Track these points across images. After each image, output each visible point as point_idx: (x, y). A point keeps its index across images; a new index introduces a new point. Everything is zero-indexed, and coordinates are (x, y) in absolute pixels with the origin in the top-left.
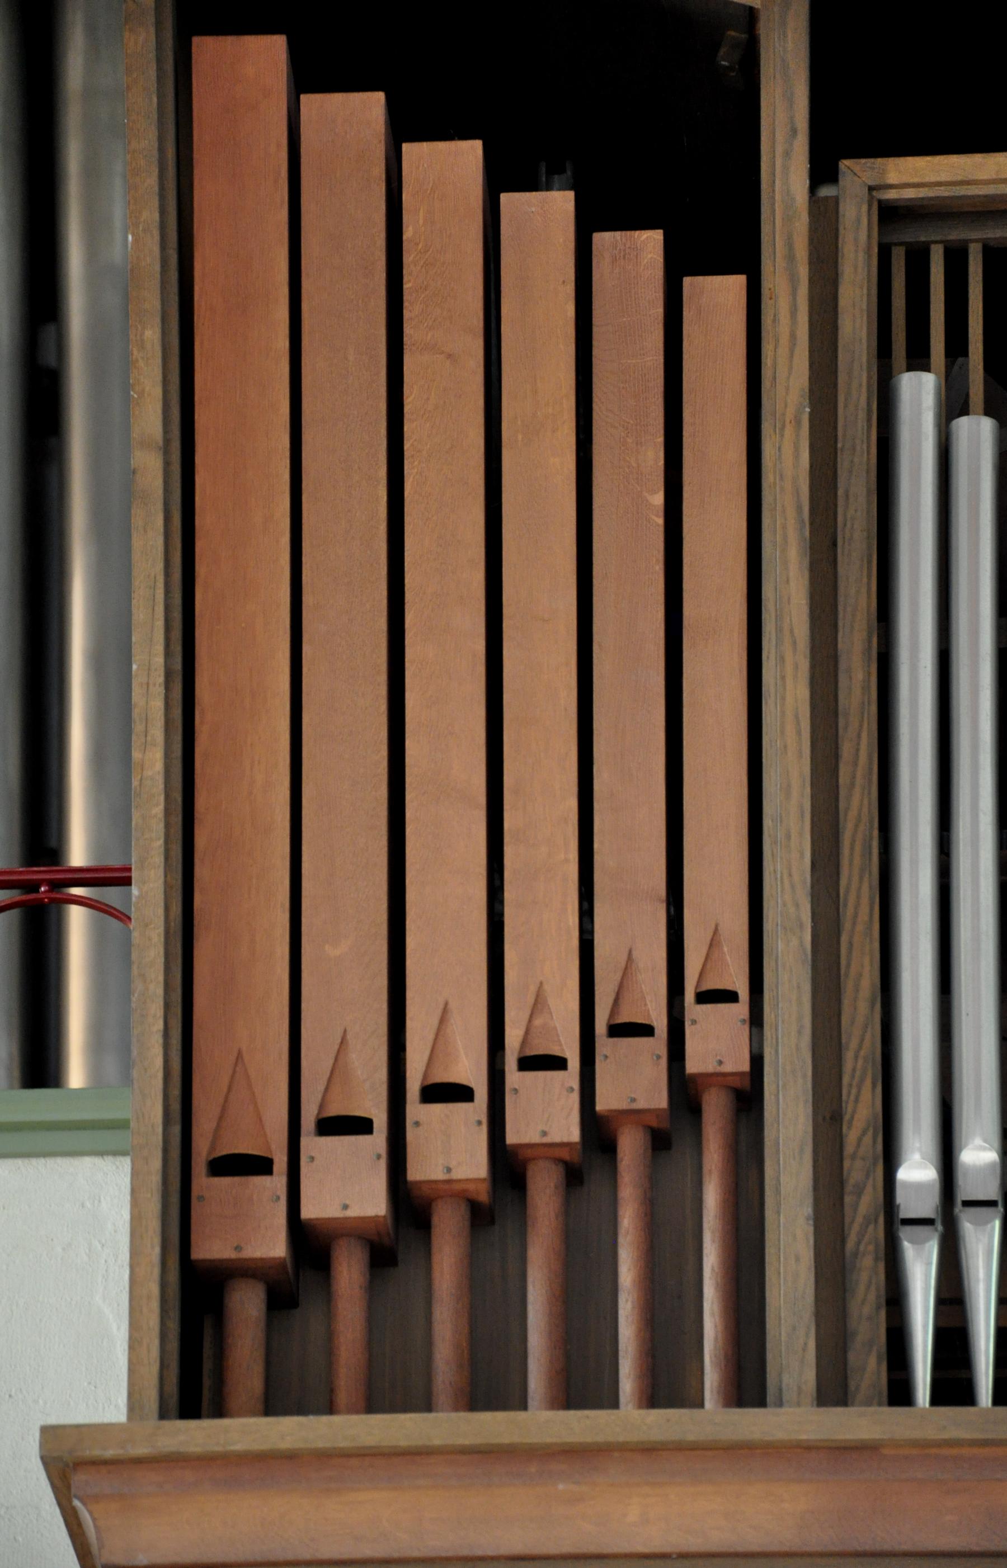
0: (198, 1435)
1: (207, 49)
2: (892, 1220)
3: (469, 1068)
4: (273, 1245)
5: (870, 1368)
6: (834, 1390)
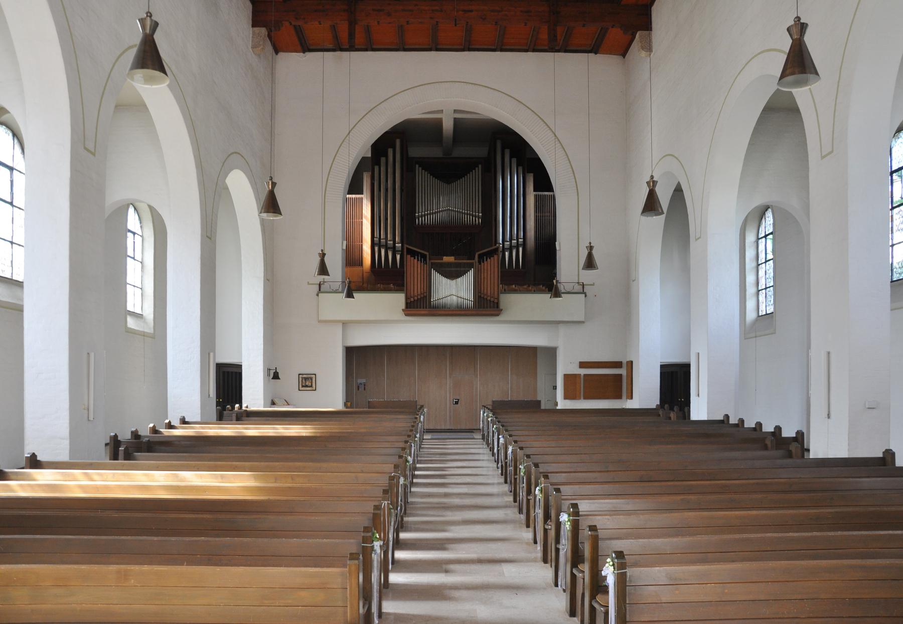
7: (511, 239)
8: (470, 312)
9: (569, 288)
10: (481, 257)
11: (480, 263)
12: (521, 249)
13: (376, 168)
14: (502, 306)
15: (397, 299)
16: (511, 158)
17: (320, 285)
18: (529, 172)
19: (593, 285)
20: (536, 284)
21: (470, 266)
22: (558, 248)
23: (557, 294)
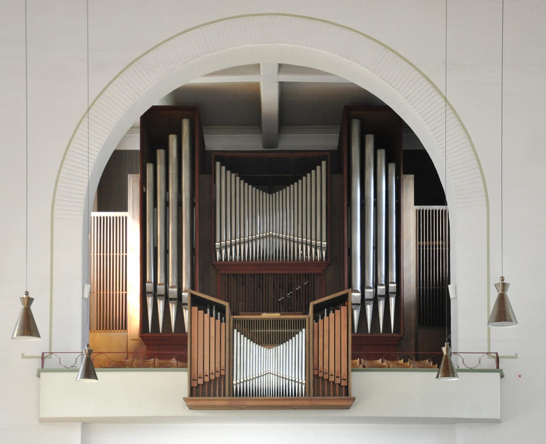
0: (192, 398)
1: (193, 308)
2: (233, 384)
3: (208, 374)
4: (196, 385)
5: (232, 394)
6: (229, 396)
7: (376, 284)
8: (299, 403)
9: (471, 361)
10: (319, 311)
11: (316, 319)
12: (392, 301)
13: (149, 168)
14: (354, 392)
15: (177, 380)
16: (376, 147)
17: (43, 358)
18: (407, 172)
19: (516, 357)
20: (418, 358)
21: (301, 325)
22: (452, 295)
23: (449, 371)
